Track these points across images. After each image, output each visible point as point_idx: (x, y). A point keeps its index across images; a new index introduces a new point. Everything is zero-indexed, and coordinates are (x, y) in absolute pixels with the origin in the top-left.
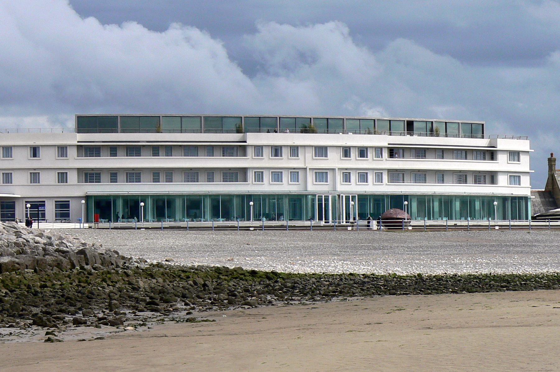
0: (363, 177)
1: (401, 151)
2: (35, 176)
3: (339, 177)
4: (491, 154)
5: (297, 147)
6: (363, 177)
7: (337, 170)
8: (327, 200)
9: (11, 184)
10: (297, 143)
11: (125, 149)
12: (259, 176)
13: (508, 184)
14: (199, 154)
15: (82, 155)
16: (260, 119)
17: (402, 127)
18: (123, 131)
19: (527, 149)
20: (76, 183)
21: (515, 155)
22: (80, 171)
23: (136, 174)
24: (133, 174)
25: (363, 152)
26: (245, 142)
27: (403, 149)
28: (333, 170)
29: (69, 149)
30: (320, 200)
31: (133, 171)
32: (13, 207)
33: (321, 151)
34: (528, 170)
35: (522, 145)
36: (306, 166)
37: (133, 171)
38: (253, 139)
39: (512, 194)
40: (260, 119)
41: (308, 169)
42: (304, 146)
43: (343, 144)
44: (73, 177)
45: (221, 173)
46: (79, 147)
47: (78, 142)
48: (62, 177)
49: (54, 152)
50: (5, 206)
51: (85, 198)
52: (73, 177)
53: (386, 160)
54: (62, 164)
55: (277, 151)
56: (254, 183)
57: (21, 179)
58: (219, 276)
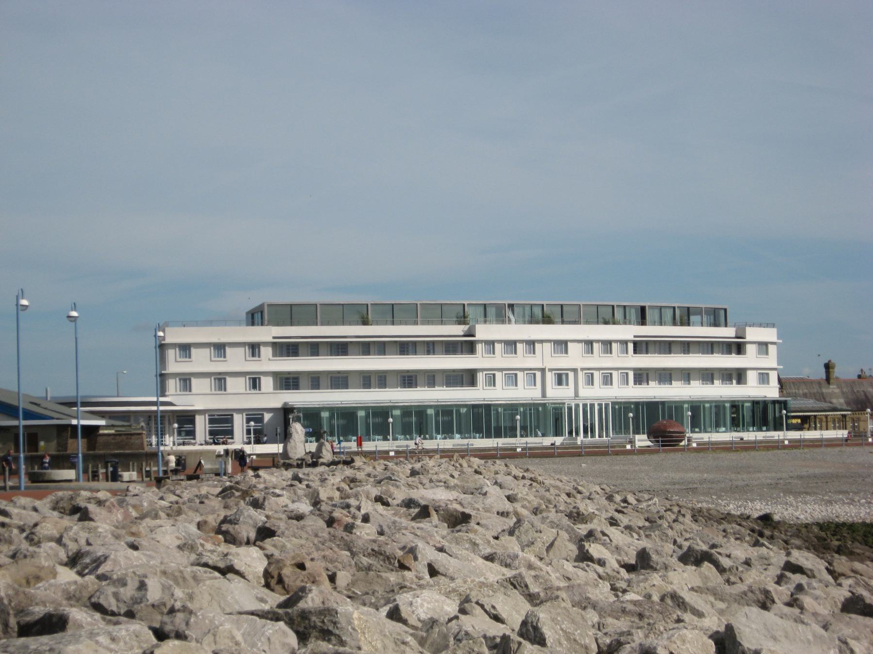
0: (512, 378)
1: (644, 345)
2: (255, 383)
3: (550, 377)
4: (738, 347)
5: (565, 343)
6: (512, 378)
7: (579, 370)
8: (592, 406)
9: (190, 393)
10: (533, 337)
11: (329, 347)
12: (492, 381)
13: (246, 390)
14: (417, 350)
15: (186, 355)
16: (291, 307)
17: (633, 315)
18: (424, 323)
19: (774, 339)
20: (271, 389)
21: (763, 346)
22: (276, 375)
23: (342, 378)
24: (339, 378)
25: (607, 345)
26: (473, 336)
27: (647, 343)
28: (575, 370)
29: (262, 349)
30: (570, 409)
31: (339, 375)
32: (192, 421)
33: (562, 345)
34: (775, 365)
35: (769, 335)
36: (544, 365)
37: (339, 375)
38: (484, 332)
39: (765, 397)
40: (291, 307)
41: (547, 370)
42: (542, 342)
43: (215, 340)
44: (267, 383)
45: (397, 376)
46: (274, 345)
47: (274, 338)
48: (255, 383)
49: (580, 347)
50: (446, 418)
51: (329, 411)
52: (267, 383)
53: (269, 360)
54: (254, 366)
55: (511, 345)
56: (485, 388)
57: (235, 385)
58: (114, 506)
